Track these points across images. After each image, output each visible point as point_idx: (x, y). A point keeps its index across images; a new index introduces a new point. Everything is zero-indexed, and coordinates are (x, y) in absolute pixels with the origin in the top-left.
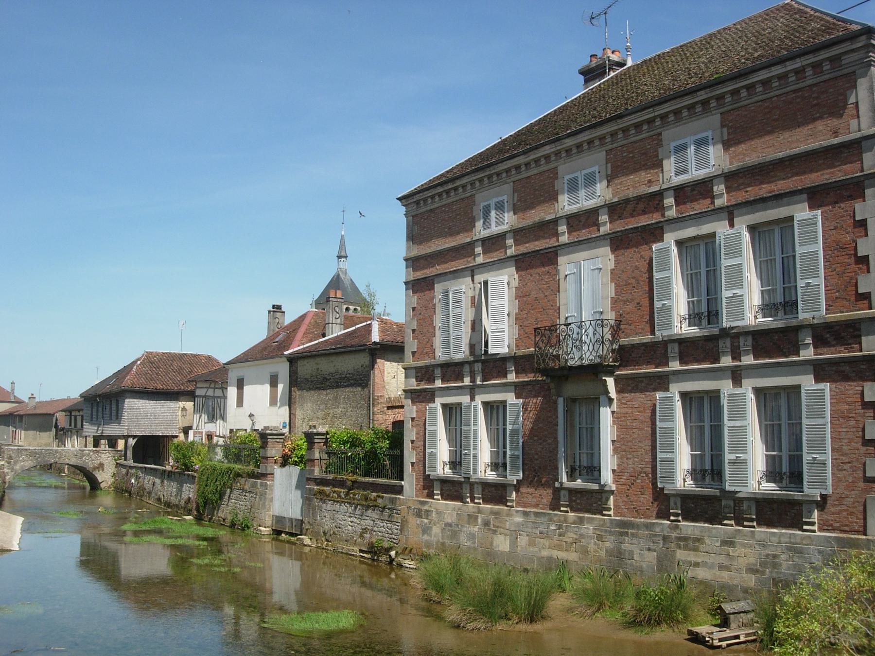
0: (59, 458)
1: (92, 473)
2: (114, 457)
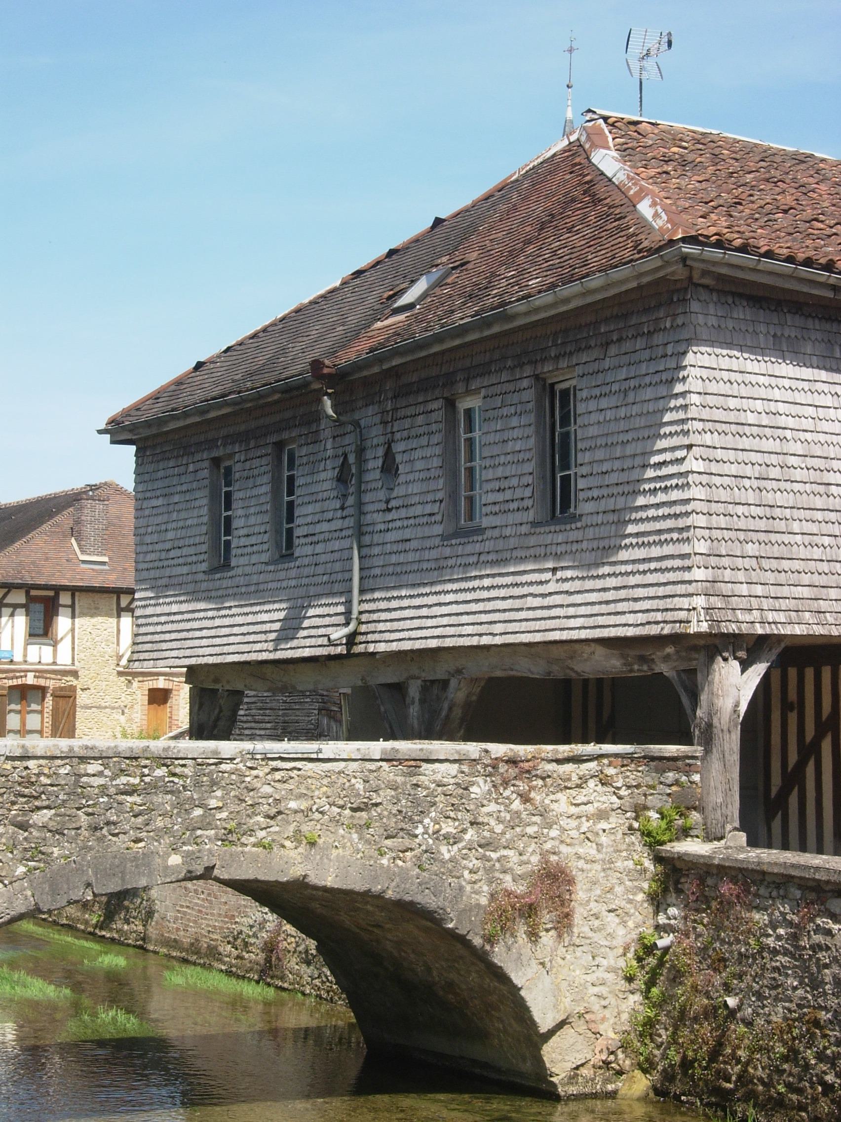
0: (228, 837)
1: (482, 958)
2: (639, 810)
